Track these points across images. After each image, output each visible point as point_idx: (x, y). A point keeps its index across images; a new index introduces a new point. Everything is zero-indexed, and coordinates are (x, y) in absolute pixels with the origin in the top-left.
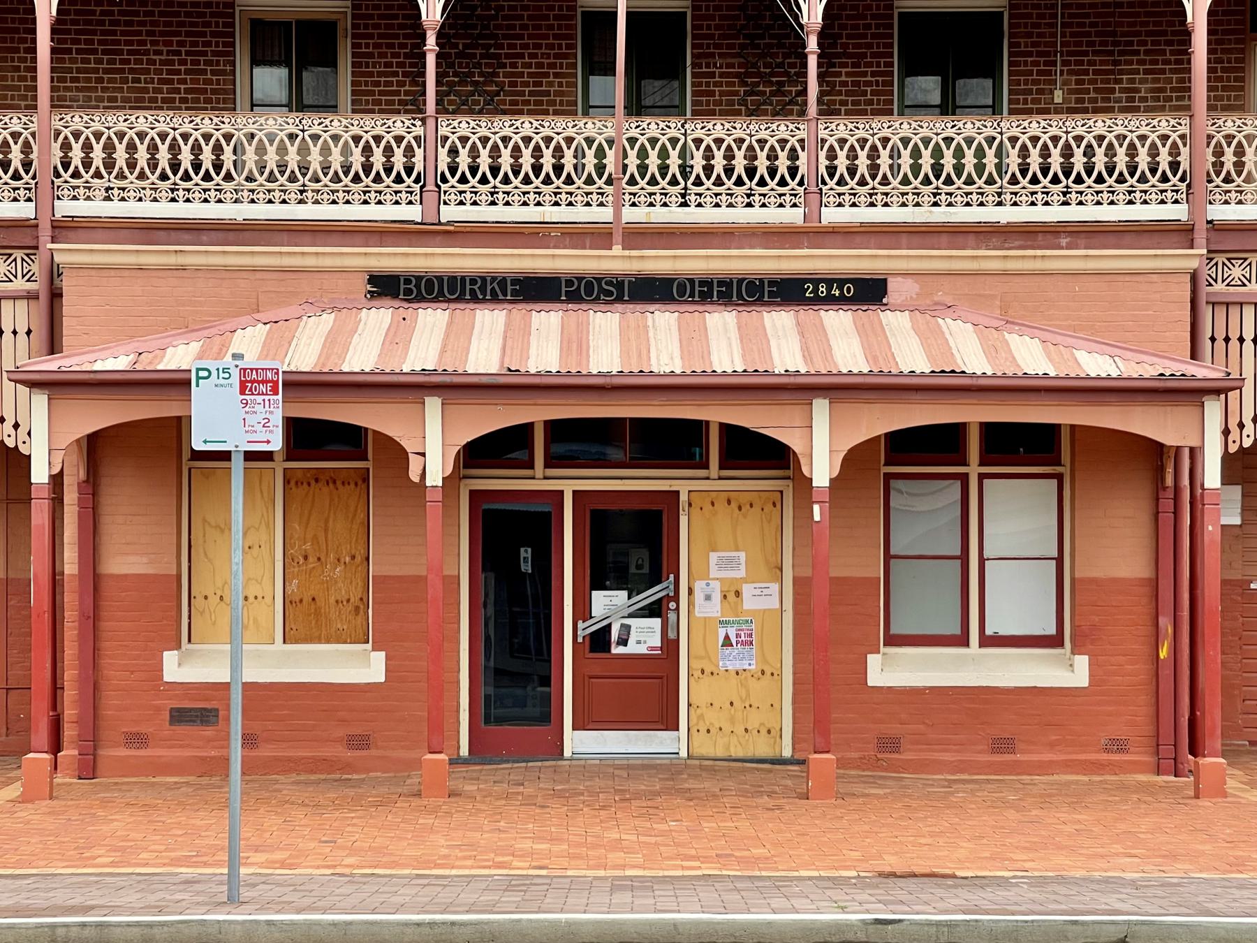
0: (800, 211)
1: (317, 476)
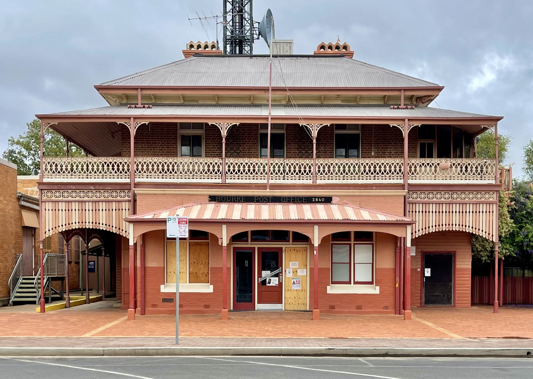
0: (311, 181)
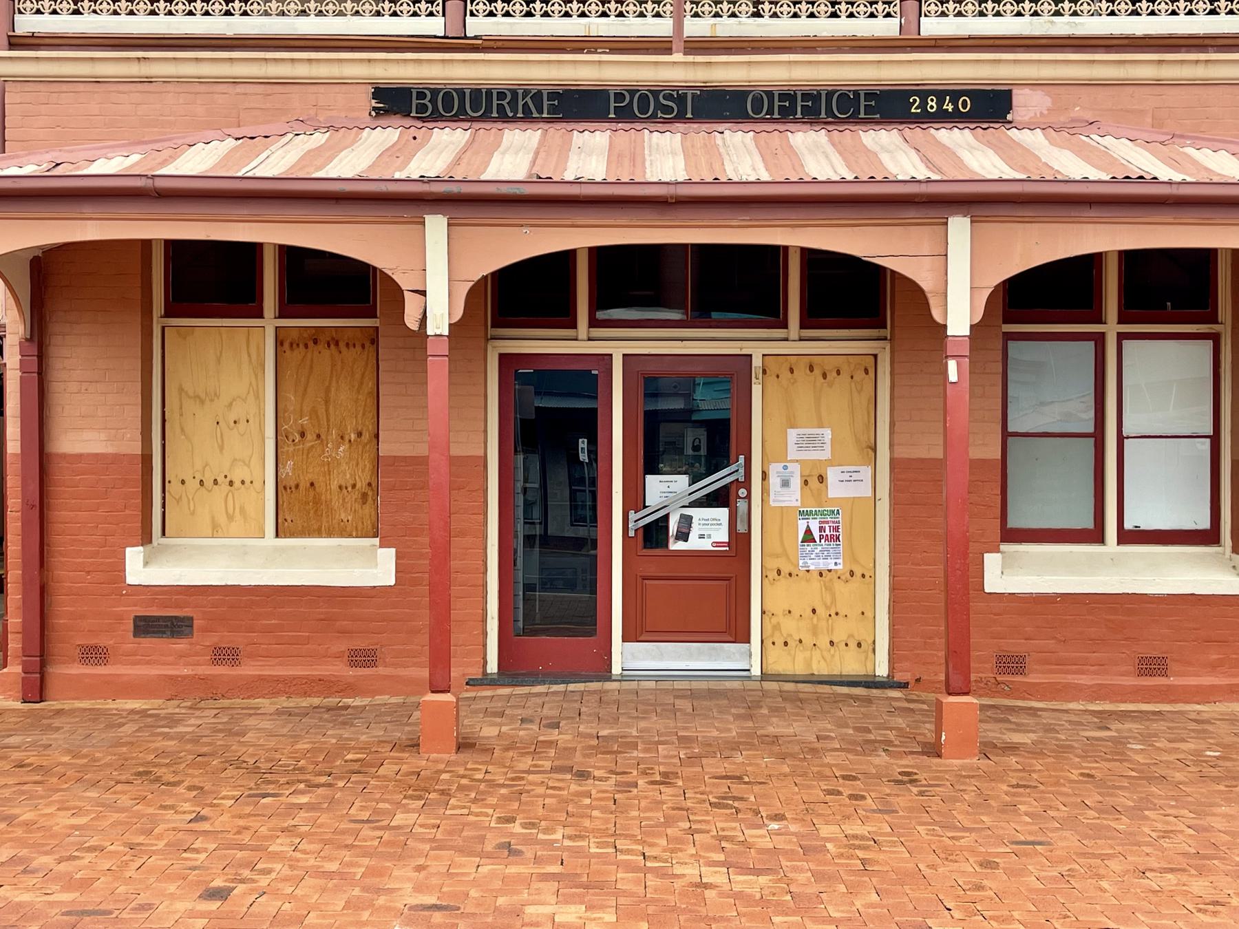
1: (315, 337)
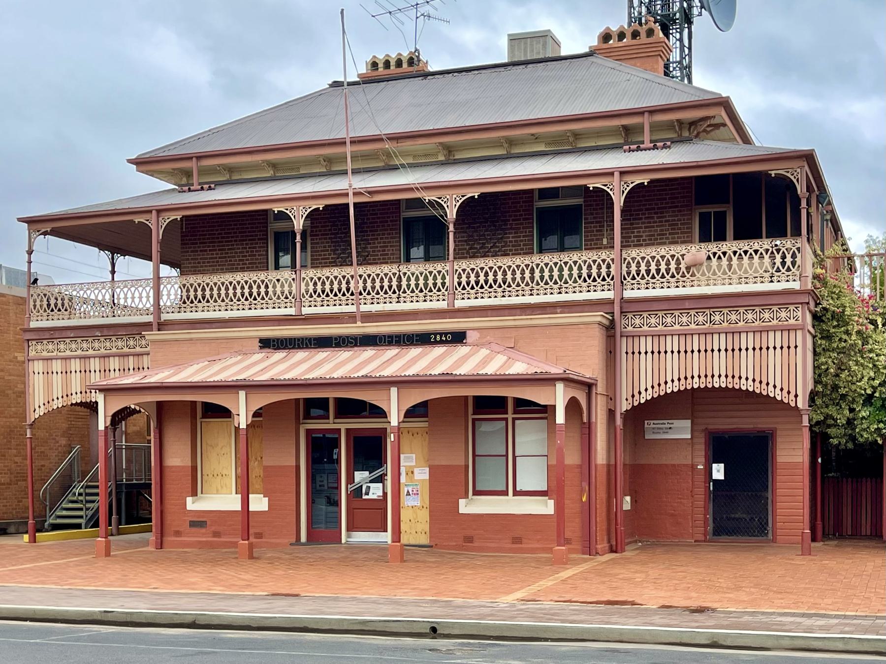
0: (446, 302)
